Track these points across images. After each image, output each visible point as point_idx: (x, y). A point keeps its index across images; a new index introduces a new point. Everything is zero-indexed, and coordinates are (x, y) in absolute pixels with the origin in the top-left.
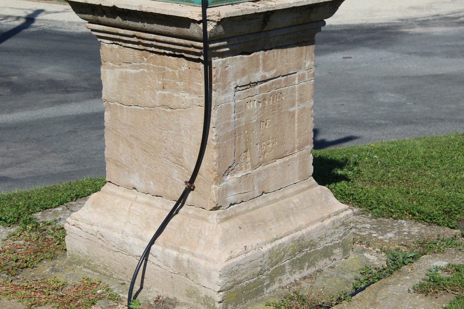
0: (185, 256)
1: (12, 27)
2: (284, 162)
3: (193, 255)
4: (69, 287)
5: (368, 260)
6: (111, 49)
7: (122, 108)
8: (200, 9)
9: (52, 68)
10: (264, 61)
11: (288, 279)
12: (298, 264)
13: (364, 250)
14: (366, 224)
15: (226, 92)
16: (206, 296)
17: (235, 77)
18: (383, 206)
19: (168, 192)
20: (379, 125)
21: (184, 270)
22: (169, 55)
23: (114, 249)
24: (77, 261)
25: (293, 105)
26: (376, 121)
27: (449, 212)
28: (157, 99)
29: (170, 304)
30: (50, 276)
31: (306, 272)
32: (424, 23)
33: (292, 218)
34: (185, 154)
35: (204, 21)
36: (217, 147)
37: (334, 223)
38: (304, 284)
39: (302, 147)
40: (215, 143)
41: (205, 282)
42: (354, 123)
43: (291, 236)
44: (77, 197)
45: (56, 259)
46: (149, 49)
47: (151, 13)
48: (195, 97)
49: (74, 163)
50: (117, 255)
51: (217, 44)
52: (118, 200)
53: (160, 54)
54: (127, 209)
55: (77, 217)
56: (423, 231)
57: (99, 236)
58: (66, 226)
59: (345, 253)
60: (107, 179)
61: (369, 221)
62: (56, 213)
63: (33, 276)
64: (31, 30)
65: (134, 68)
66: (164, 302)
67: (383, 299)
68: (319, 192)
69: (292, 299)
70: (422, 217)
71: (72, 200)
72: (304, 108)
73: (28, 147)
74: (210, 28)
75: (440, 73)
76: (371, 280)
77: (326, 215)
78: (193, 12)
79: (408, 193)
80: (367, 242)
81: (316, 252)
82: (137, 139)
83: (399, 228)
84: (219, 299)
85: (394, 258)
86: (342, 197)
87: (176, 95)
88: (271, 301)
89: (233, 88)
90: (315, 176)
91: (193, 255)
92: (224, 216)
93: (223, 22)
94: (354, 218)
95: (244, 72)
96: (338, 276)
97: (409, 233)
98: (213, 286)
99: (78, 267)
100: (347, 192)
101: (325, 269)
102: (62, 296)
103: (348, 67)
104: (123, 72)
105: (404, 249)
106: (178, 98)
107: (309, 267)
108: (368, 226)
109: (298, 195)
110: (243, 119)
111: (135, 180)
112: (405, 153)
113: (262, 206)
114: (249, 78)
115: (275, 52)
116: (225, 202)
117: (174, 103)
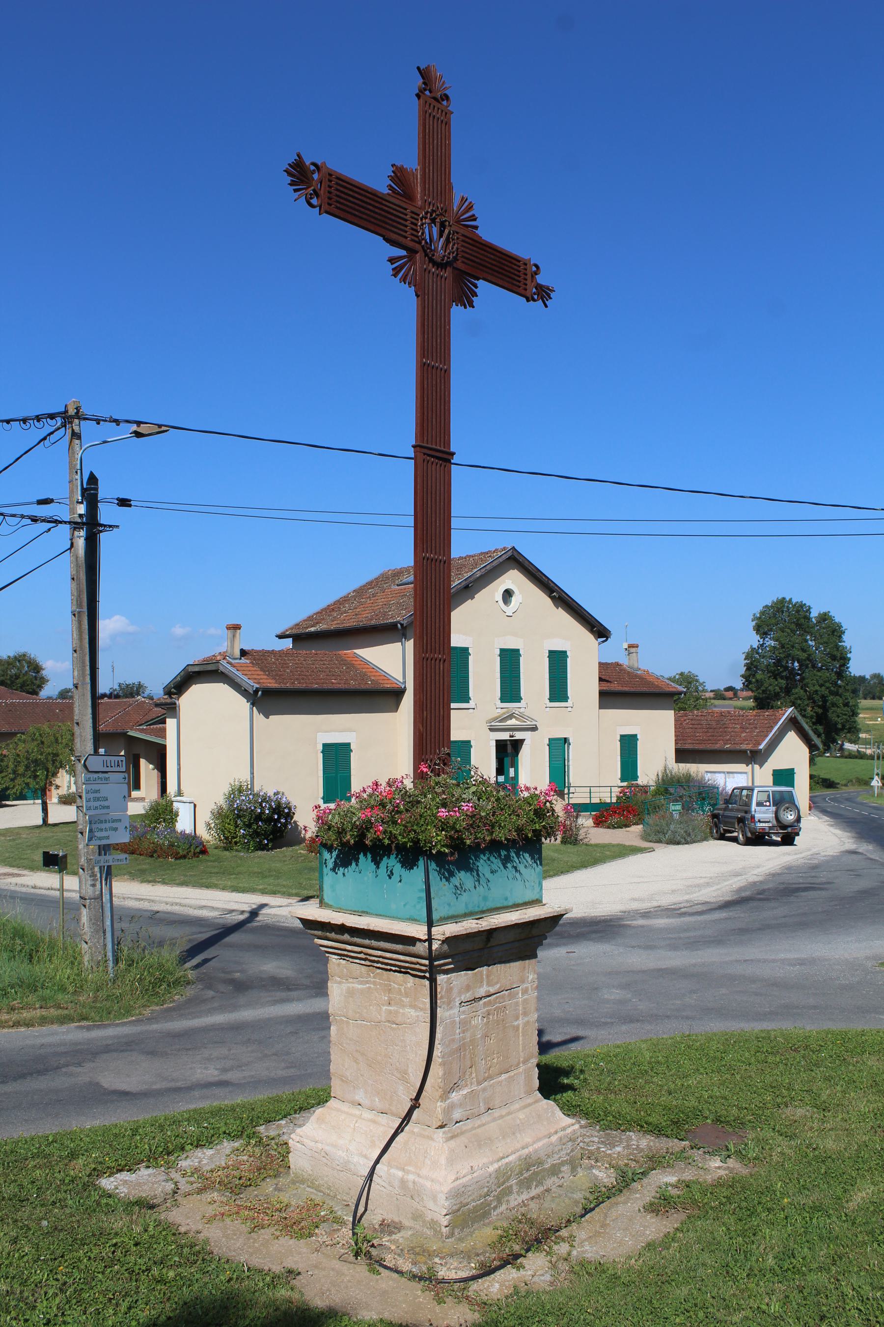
0: (411, 1177)
1: (236, 922)
2: (509, 1077)
3: (419, 1175)
4: (292, 1209)
5: (596, 1177)
6: (339, 965)
7: (348, 1023)
8: (425, 928)
9: (274, 964)
10: (488, 976)
11: (515, 1200)
12: (526, 1184)
13: (592, 1167)
14: (594, 1137)
15: (451, 1008)
16: (432, 1220)
17: (460, 993)
18: (610, 1118)
19: (393, 1109)
20: (606, 1024)
21: (409, 1191)
22: (395, 971)
23: (338, 1168)
24: (300, 1180)
25: (517, 1019)
26: (603, 1020)
27: (677, 1123)
28: (383, 1015)
29: (395, 1228)
30: (274, 1196)
31: (534, 1192)
32: (646, 915)
33: (519, 1136)
34: (410, 1070)
35: (430, 940)
36: (443, 1064)
37: (561, 1139)
38: (533, 1205)
39: (527, 1061)
40: (440, 1060)
41: (431, 1205)
42: (580, 1022)
43: (517, 1154)
44: (301, 1109)
45: (279, 1177)
46: (375, 965)
47: (378, 932)
48: (421, 1013)
49: (295, 1067)
50: (342, 1174)
51: (442, 962)
52: (343, 1117)
53: (386, 970)
54: (352, 1126)
55: (301, 1134)
56: (652, 1144)
57: (323, 1154)
58: (290, 1141)
59: (574, 1169)
60: (332, 1095)
61: (597, 1134)
62: (279, 1126)
63: (256, 1196)
64: (255, 924)
65: (361, 983)
66: (389, 1226)
67: (613, 1220)
68: (545, 1107)
69: (520, 1222)
70: (650, 1128)
71: (295, 1113)
72: (528, 1022)
73: (249, 1049)
74: (435, 946)
75: (664, 967)
76: (601, 1200)
77: (552, 1131)
78: (418, 931)
79: (635, 1103)
80: (594, 1156)
81: (544, 1170)
82: (363, 1054)
83: (627, 1142)
84: (446, 1223)
85: (623, 1174)
86: (569, 1110)
87: (401, 1011)
88: (499, 1224)
89: (457, 1004)
90: (541, 1090)
91: (419, 1175)
92: (450, 1135)
93: (447, 941)
94: (582, 1130)
95: (468, 988)
96: (566, 1196)
97: (638, 1146)
98: (439, 1210)
99: (302, 1186)
100: (574, 1103)
101: (554, 1188)
102: (286, 1218)
103: (573, 963)
104: (348, 987)
105: (633, 1164)
106: (403, 1014)
107: (536, 1186)
108: (596, 1139)
109: (525, 1111)
110: (468, 1034)
111: (360, 1096)
112: (631, 1058)
113: (488, 1123)
114: (473, 993)
115: (498, 966)
116: (450, 1120)
117: (399, 1020)
